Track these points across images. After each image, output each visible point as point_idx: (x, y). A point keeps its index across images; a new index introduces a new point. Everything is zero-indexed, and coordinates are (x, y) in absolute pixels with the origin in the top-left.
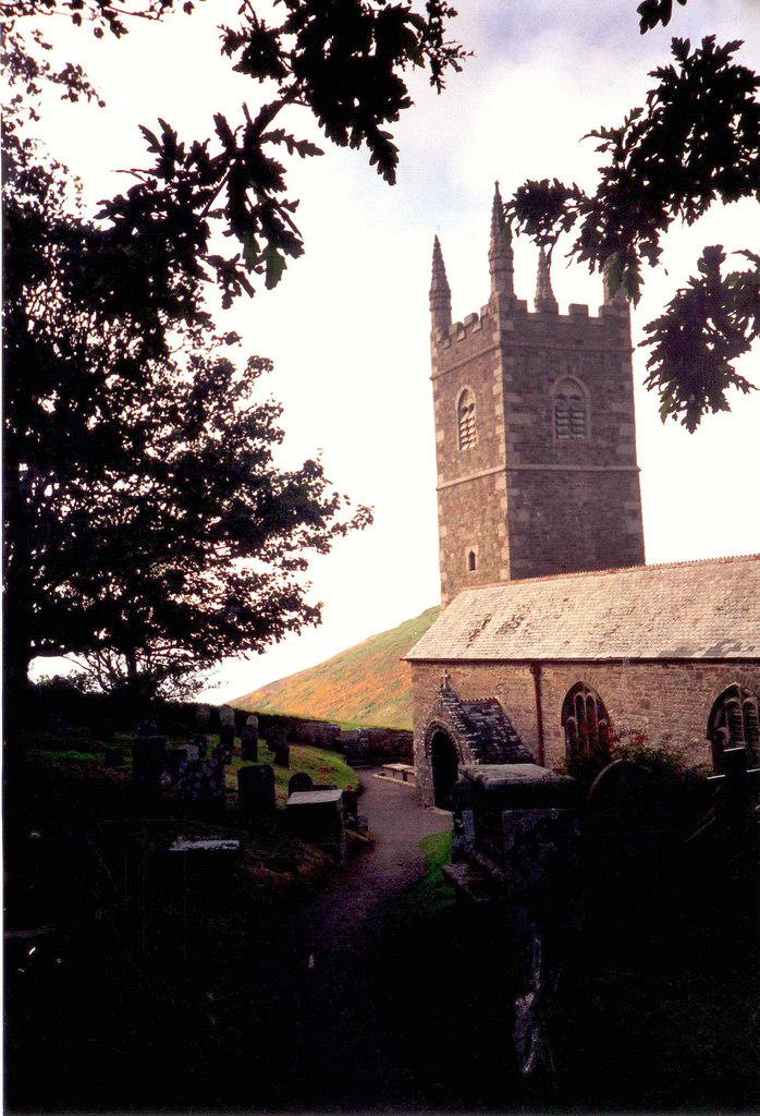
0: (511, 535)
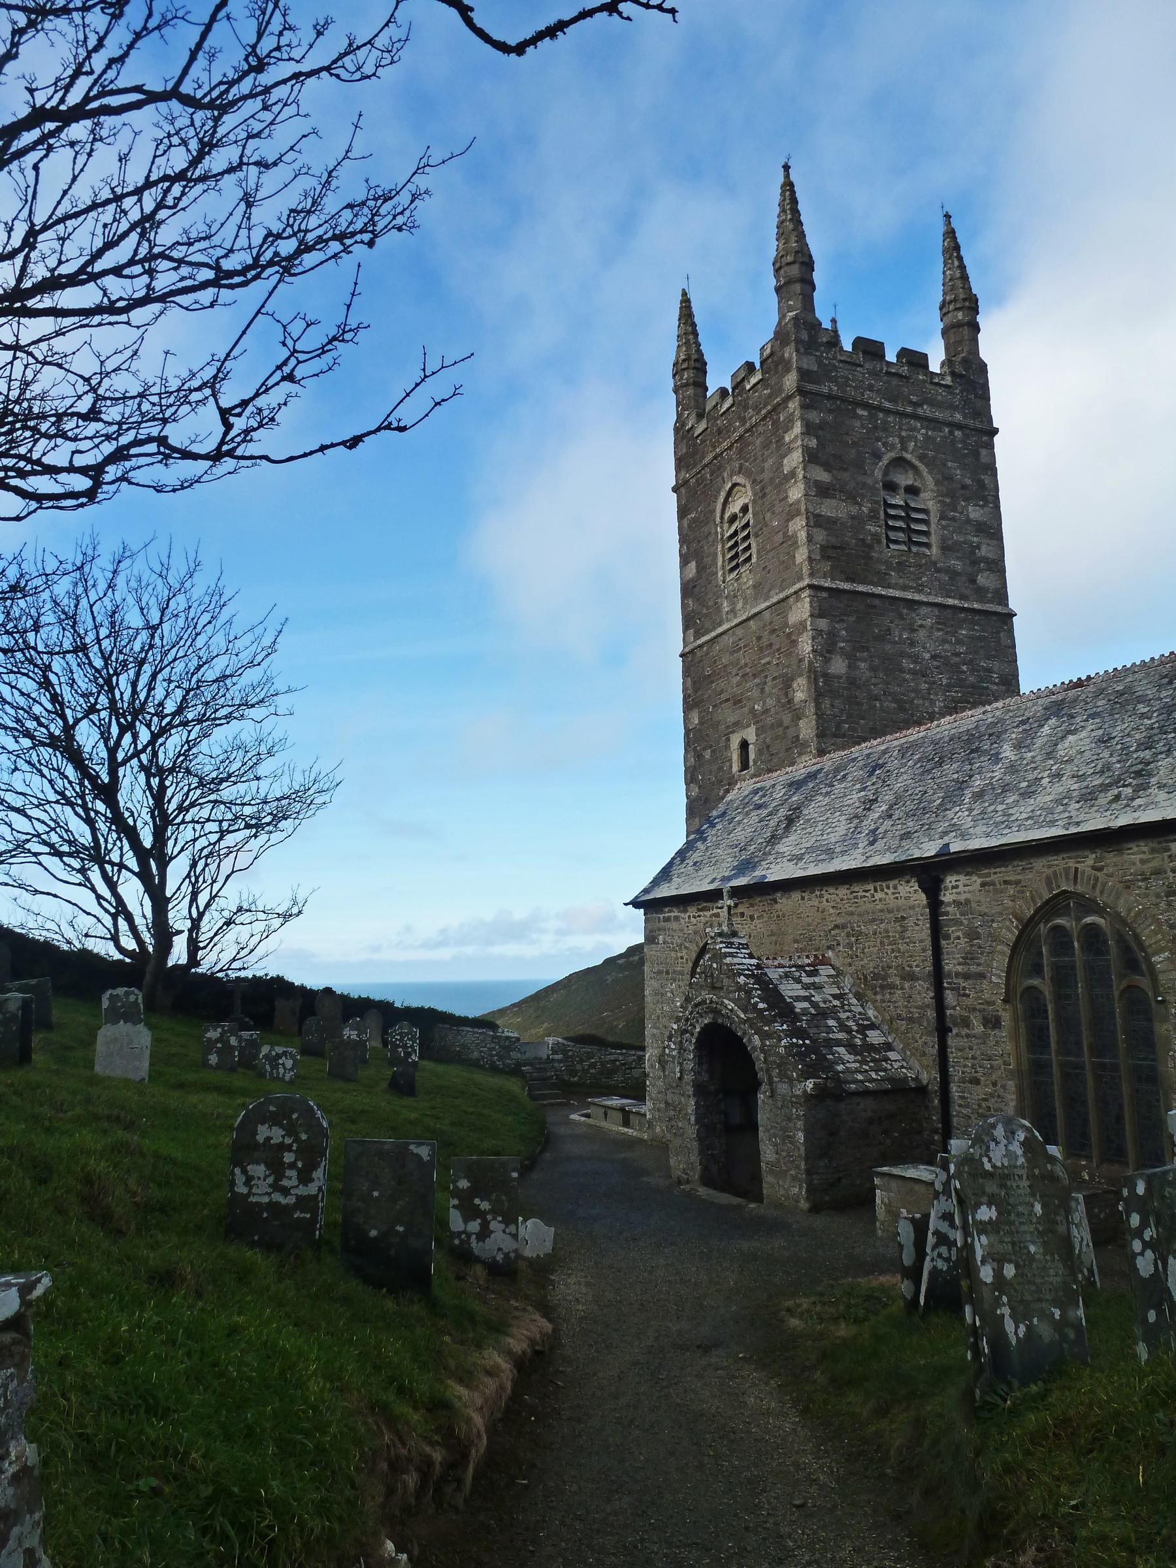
0: (818, 696)
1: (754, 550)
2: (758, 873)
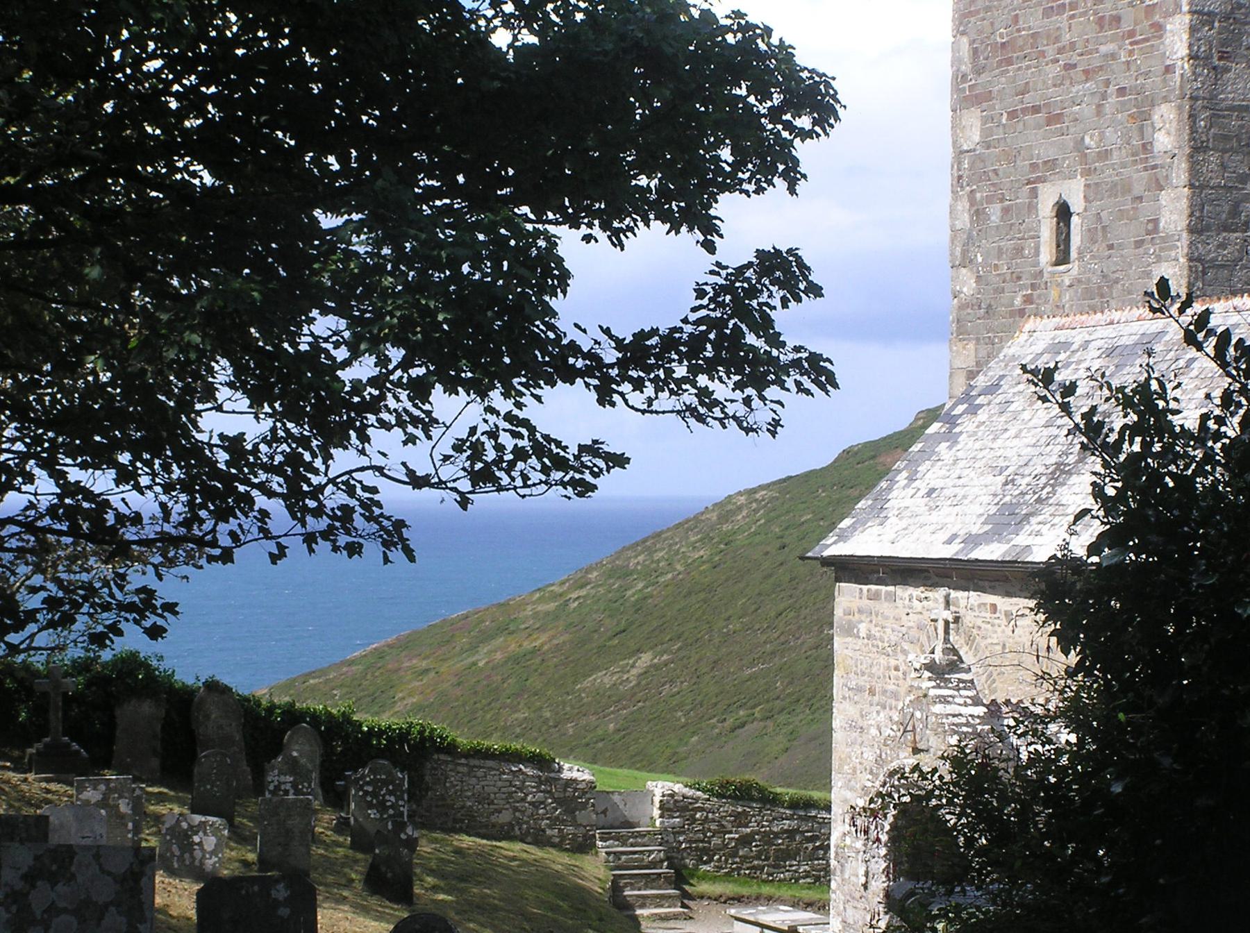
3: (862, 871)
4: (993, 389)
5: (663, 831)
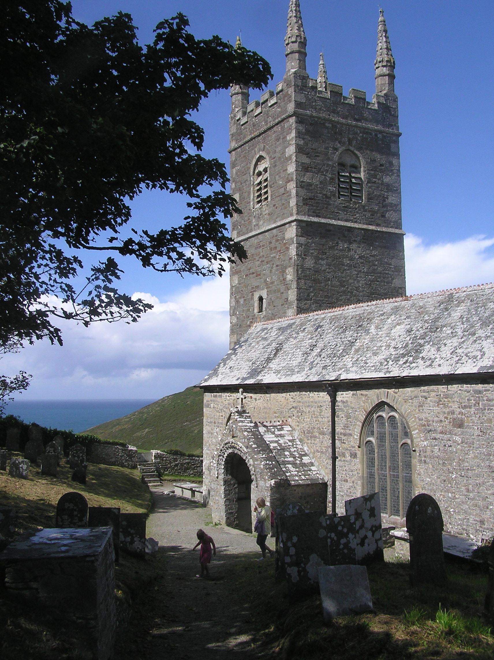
1: (269, 194)
2: (259, 378)
3: (216, 473)
4: (246, 341)
5: (155, 463)
